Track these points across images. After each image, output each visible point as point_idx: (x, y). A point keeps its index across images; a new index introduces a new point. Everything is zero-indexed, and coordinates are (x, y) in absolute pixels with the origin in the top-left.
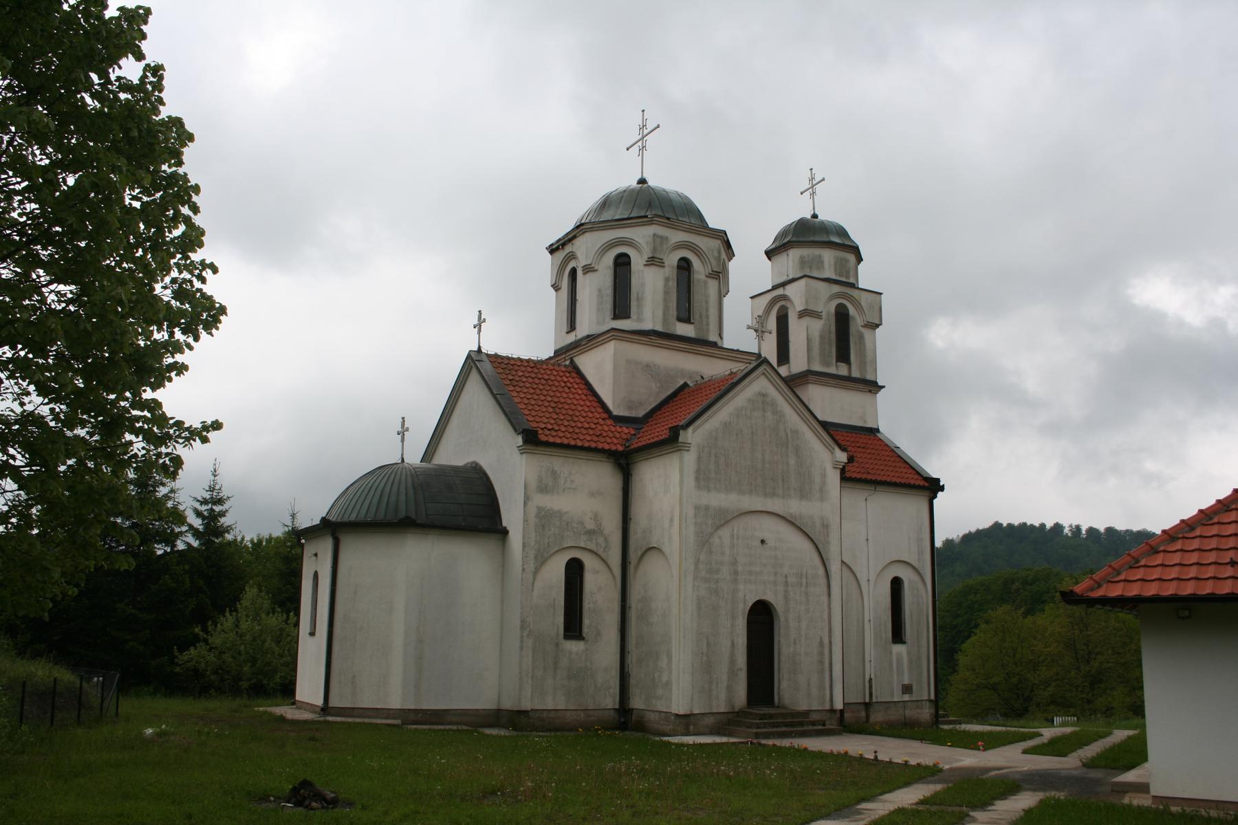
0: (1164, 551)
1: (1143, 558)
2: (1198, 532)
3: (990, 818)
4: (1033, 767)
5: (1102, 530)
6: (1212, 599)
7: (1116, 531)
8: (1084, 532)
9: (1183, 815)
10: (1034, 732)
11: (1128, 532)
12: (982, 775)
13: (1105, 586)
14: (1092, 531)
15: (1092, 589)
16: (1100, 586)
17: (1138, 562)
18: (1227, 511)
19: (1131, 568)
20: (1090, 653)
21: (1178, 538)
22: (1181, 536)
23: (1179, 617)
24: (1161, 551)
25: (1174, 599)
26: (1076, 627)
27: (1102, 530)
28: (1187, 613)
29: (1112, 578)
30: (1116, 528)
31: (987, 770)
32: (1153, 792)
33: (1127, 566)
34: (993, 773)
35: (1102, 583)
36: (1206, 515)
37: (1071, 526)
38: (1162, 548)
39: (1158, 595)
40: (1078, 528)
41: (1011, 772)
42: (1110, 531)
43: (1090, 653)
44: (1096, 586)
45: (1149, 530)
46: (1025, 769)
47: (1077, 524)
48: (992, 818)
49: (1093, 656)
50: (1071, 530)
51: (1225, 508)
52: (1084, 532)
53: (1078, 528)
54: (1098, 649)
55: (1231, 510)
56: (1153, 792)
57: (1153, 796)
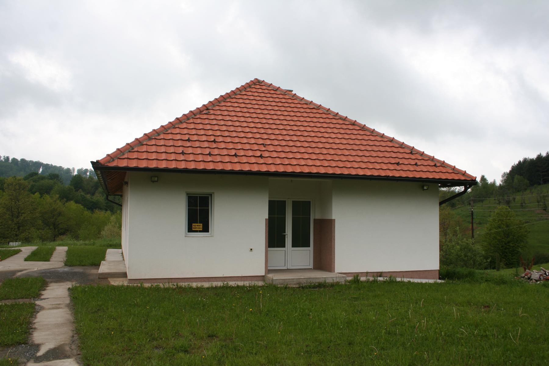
0: (146, 145)
1: (135, 147)
2: (162, 136)
3: (51, 305)
4: (39, 269)
5: (19, 160)
6: (176, 171)
7: (26, 160)
8: (10, 160)
9: (150, 288)
10: (17, 250)
11: (31, 162)
12: (13, 276)
13: (116, 160)
14: (14, 160)
15: (109, 162)
16: (113, 160)
17: (133, 149)
18: (174, 128)
19: (130, 152)
20: (19, 213)
21: (153, 139)
22: (154, 137)
23: (152, 181)
24: (145, 144)
25: (146, 169)
26: (13, 200)
27: (19, 160)
28: (156, 179)
29: (120, 156)
30: (26, 159)
31: (14, 272)
32: (129, 277)
33: (127, 151)
34: (19, 274)
35: (115, 159)
36: (165, 129)
37: (4, 157)
38: (145, 143)
39: (147, 167)
40: (8, 158)
41: (23, 275)
42: (23, 160)
43: (19, 213)
44: (112, 160)
45: (41, 161)
46: (36, 269)
47: (7, 156)
48: (53, 305)
49: (20, 214)
50: (4, 158)
51: (173, 127)
52: (10, 160)
53: (8, 158)
54: (23, 211)
55: (176, 128)
56: (129, 277)
57: (129, 279)
